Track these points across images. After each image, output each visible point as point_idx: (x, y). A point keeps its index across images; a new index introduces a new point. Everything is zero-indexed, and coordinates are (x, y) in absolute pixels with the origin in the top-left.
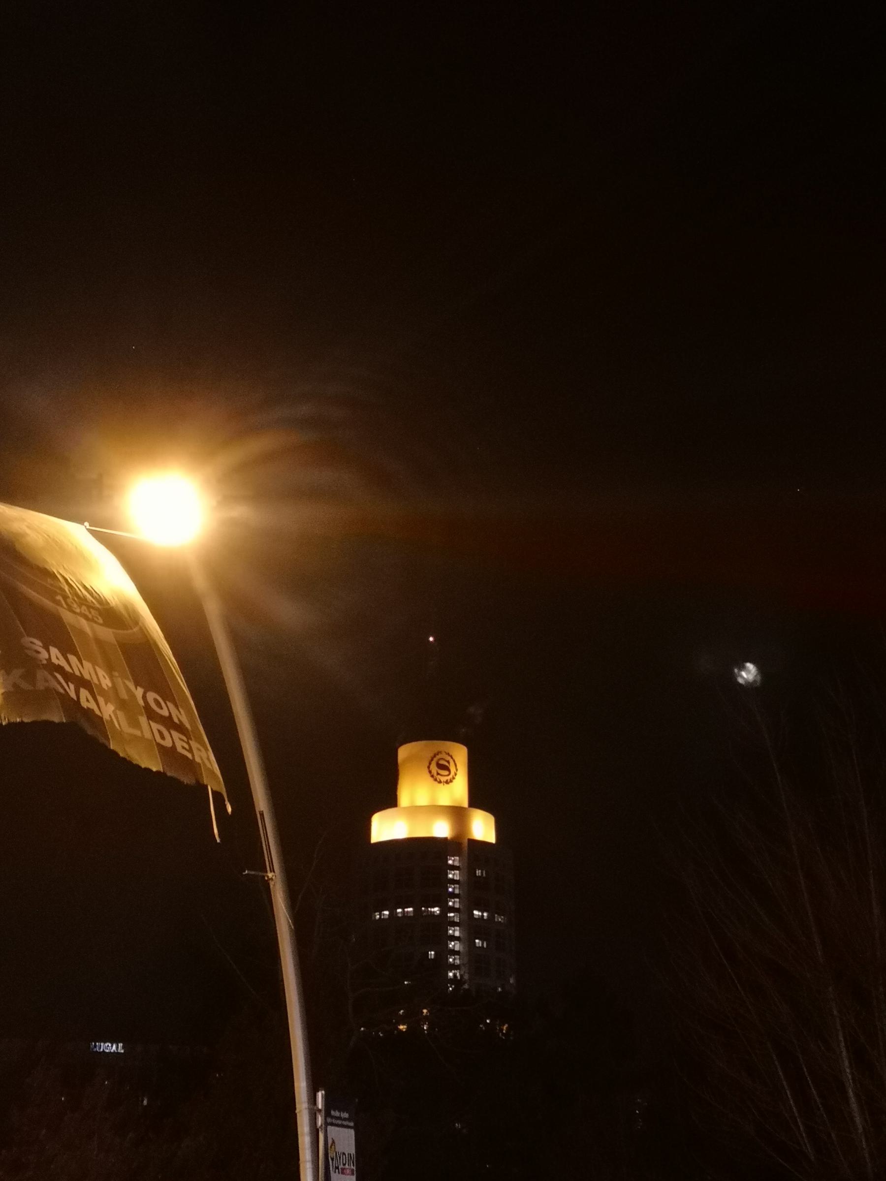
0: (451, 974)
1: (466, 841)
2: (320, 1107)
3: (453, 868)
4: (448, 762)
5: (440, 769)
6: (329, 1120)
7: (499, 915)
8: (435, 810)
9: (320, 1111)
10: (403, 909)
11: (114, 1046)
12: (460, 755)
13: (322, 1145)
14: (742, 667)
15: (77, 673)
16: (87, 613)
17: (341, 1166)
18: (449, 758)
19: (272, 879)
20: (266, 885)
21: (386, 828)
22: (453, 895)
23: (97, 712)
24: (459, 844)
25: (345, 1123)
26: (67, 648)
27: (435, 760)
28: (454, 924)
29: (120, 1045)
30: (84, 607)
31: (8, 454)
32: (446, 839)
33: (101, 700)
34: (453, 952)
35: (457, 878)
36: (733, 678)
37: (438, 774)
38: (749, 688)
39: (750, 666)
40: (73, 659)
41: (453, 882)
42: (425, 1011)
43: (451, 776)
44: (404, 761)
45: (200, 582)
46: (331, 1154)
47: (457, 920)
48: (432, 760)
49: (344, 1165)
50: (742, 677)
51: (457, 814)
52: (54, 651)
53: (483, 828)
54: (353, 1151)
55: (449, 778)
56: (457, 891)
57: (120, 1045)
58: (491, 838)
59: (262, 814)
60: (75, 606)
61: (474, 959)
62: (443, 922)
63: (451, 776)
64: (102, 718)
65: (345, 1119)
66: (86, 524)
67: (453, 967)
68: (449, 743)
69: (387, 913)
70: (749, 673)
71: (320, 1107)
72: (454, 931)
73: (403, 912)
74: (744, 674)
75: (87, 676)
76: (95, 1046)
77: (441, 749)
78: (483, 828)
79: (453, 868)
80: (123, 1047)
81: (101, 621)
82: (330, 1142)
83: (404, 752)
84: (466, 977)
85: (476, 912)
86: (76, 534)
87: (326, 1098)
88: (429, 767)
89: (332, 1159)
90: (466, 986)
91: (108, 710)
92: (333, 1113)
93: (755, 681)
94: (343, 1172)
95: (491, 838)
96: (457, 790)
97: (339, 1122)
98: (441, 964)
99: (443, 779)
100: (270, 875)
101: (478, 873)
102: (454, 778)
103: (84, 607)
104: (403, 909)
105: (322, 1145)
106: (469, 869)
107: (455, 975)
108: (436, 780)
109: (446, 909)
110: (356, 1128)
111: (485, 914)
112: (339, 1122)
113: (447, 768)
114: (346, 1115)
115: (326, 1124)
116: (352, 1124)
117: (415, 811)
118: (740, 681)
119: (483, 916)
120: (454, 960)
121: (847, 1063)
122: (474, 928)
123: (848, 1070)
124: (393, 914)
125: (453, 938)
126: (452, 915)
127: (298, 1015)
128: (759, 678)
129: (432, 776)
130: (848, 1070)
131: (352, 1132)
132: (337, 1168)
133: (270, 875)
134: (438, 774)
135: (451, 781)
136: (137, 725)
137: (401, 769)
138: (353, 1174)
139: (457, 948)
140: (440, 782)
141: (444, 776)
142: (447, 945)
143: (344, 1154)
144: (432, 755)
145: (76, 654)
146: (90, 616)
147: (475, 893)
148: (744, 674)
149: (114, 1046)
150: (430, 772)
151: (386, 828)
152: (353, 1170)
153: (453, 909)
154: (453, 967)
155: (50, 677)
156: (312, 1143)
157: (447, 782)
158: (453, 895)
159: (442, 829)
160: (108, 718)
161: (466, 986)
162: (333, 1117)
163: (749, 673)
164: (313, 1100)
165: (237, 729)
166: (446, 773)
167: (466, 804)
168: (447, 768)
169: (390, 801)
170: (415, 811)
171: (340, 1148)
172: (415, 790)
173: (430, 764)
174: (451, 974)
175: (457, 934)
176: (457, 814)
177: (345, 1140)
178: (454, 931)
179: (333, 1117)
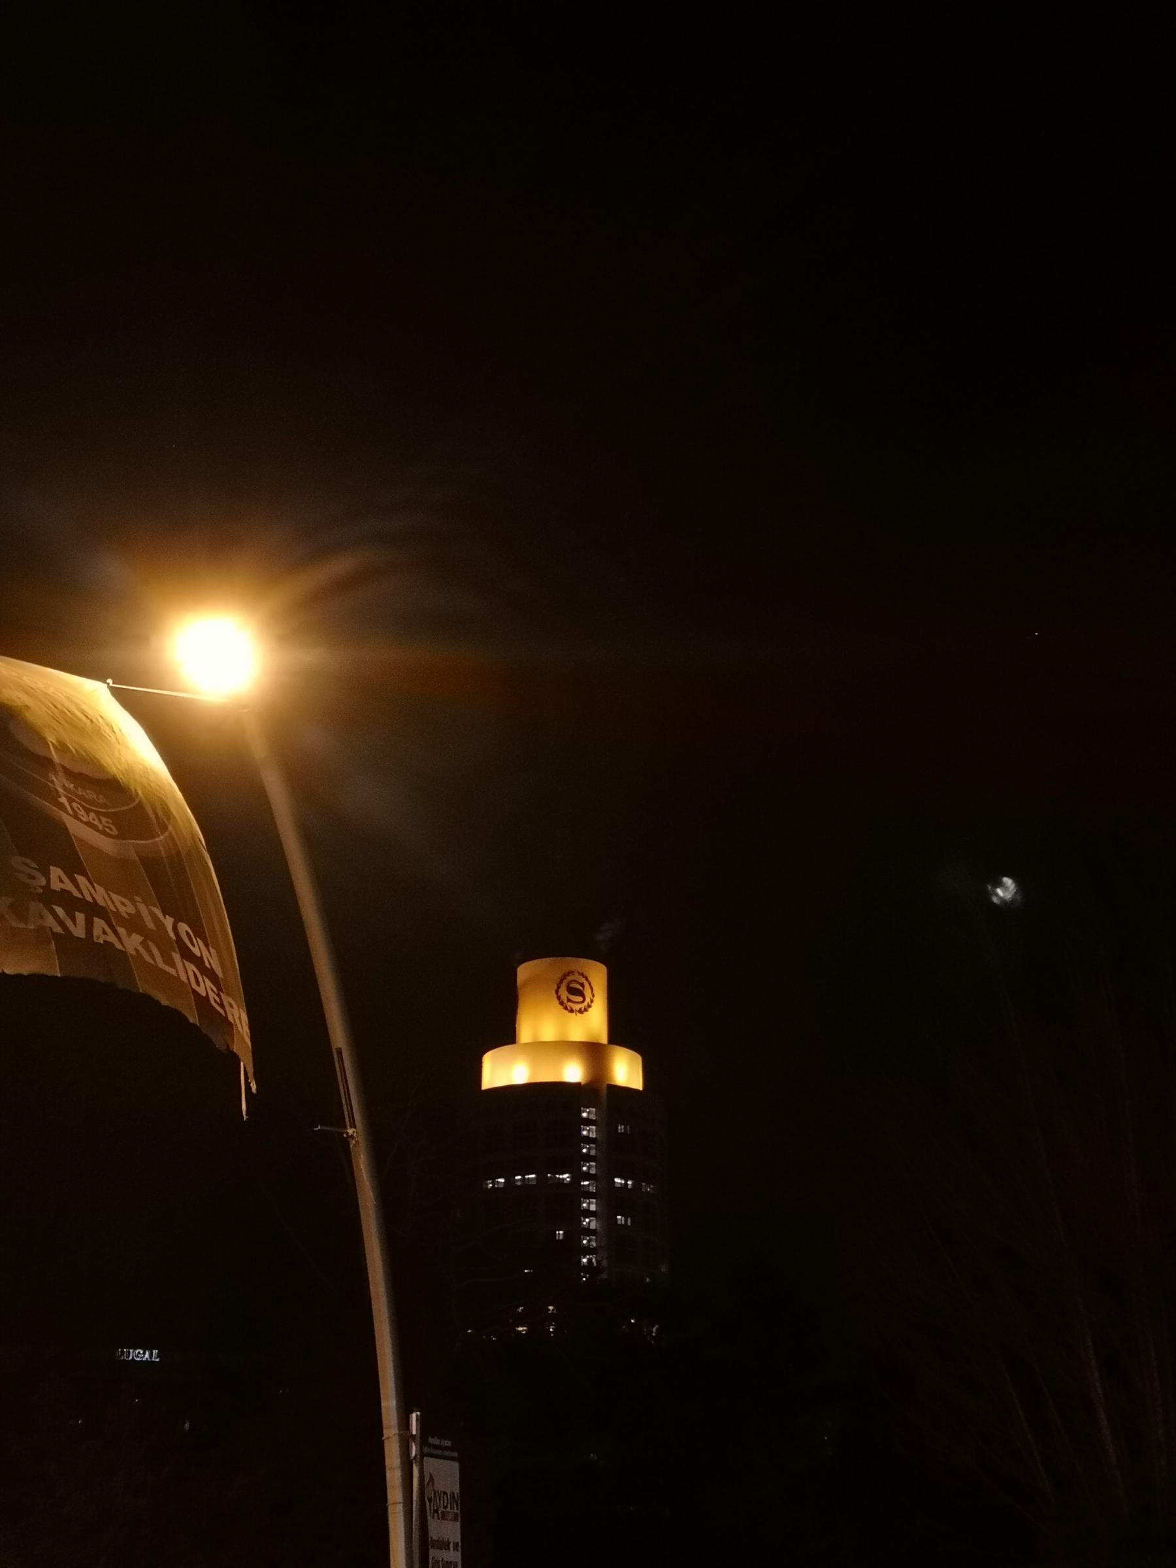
0: (585, 1260)
1: (605, 1087)
2: (414, 1432)
3: (588, 1122)
4: (582, 985)
5: (571, 994)
6: (426, 1450)
7: (648, 1184)
8: (565, 1047)
9: (414, 1437)
10: (523, 1176)
11: (147, 1355)
12: (597, 976)
13: (413, 1479)
14: (1000, 884)
15: (90, 899)
16: (96, 823)
17: (441, 1509)
18: (583, 980)
19: (352, 1137)
20: (345, 1142)
21: (502, 1070)
22: (588, 1158)
23: (119, 947)
24: (597, 1090)
25: (447, 1453)
26: (74, 867)
27: (565, 982)
28: (589, 1195)
29: (155, 1352)
30: (92, 815)
31: (21, 589)
32: (579, 1084)
33: (122, 931)
34: (588, 1232)
35: (593, 1135)
36: (987, 897)
37: (569, 1000)
38: (1006, 907)
39: (1008, 881)
40: (81, 879)
41: (588, 1140)
42: (551, 1308)
43: (585, 1004)
44: (525, 984)
45: (259, 750)
46: (429, 1493)
47: (593, 1189)
48: (561, 981)
49: (445, 1507)
50: (997, 895)
51: (594, 1053)
52: (56, 872)
53: (626, 1070)
54: (457, 1489)
55: (582, 1006)
56: (593, 1153)
57: (155, 1352)
58: (637, 1083)
59: (340, 1052)
60: (82, 812)
61: (613, 1237)
62: (575, 1193)
63: (585, 1004)
64: (124, 953)
65: (446, 1448)
66: (110, 681)
67: (587, 1250)
68: (581, 960)
69: (502, 1180)
70: (1006, 890)
71: (414, 1432)
72: (589, 1204)
73: (523, 1179)
74: (999, 891)
75: (101, 903)
76: (123, 1353)
77: (573, 968)
78: (626, 1070)
79: (588, 1122)
80: (159, 1356)
81: (115, 832)
82: (427, 1479)
83: (524, 972)
84: (605, 1263)
85: (617, 1180)
86: (94, 696)
87: (421, 1421)
88: (557, 992)
89: (430, 1501)
90: (604, 1276)
91: (132, 943)
92: (431, 1440)
93: (1013, 901)
94: (444, 1516)
95: (637, 1083)
96: (594, 1021)
97: (439, 1452)
98: (572, 1248)
99: (577, 1007)
100: (350, 1131)
101: (621, 1128)
102: (589, 1006)
103: (92, 815)
104: (523, 1176)
105: (413, 1479)
106: (607, 1122)
107: (590, 1261)
108: (566, 1008)
109: (578, 1176)
110: (460, 1460)
111: (629, 1183)
112: (439, 1452)
113: (580, 993)
114: (447, 1443)
115: (422, 1455)
116: (455, 1454)
117: (540, 1048)
118: (995, 900)
119: (626, 1184)
120: (589, 1241)
121: (1096, 1375)
122: (613, 1201)
123: (1098, 1384)
124: (510, 1181)
125: (588, 1213)
126: (586, 1183)
127: (390, 1346)
128: (1018, 897)
129: (562, 1003)
130: (1098, 1384)
131: (456, 1465)
132: (436, 1511)
133: (350, 1131)
134: (569, 1000)
135: (586, 1010)
136: (172, 964)
137: (520, 992)
138: (456, 1520)
139: (593, 1226)
140: (572, 1011)
141: (576, 1002)
142: (580, 1222)
143: (445, 1493)
144: (560, 975)
145: (85, 874)
146: (100, 827)
147: (615, 1155)
148: (999, 891)
149: (147, 1355)
150: (559, 998)
151: (502, 1070)
152: (456, 1514)
153: (587, 1176)
154: (587, 1250)
155: (46, 912)
156: (404, 1480)
157: (580, 1011)
158: (588, 1158)
159: (573, 1072)
160: (134, 953)
161: (604, 1276)
162: (430, 1445)
163: (1006, 890)
164: (405, 1423)
165: (311, 961)
166: (580, 999)
167: (604, 1040)
168: (580, 993)
169: (506, 1035)
170: (540, 1048)
171: (440, 1486)
172: (540, 1022)
173: (559, 987)
174: (585, 1260)
175: (593, 1208)
176: (594, 1053)
177: (447, 1475)
178: (589, 1204)
179: (430, 1445)
